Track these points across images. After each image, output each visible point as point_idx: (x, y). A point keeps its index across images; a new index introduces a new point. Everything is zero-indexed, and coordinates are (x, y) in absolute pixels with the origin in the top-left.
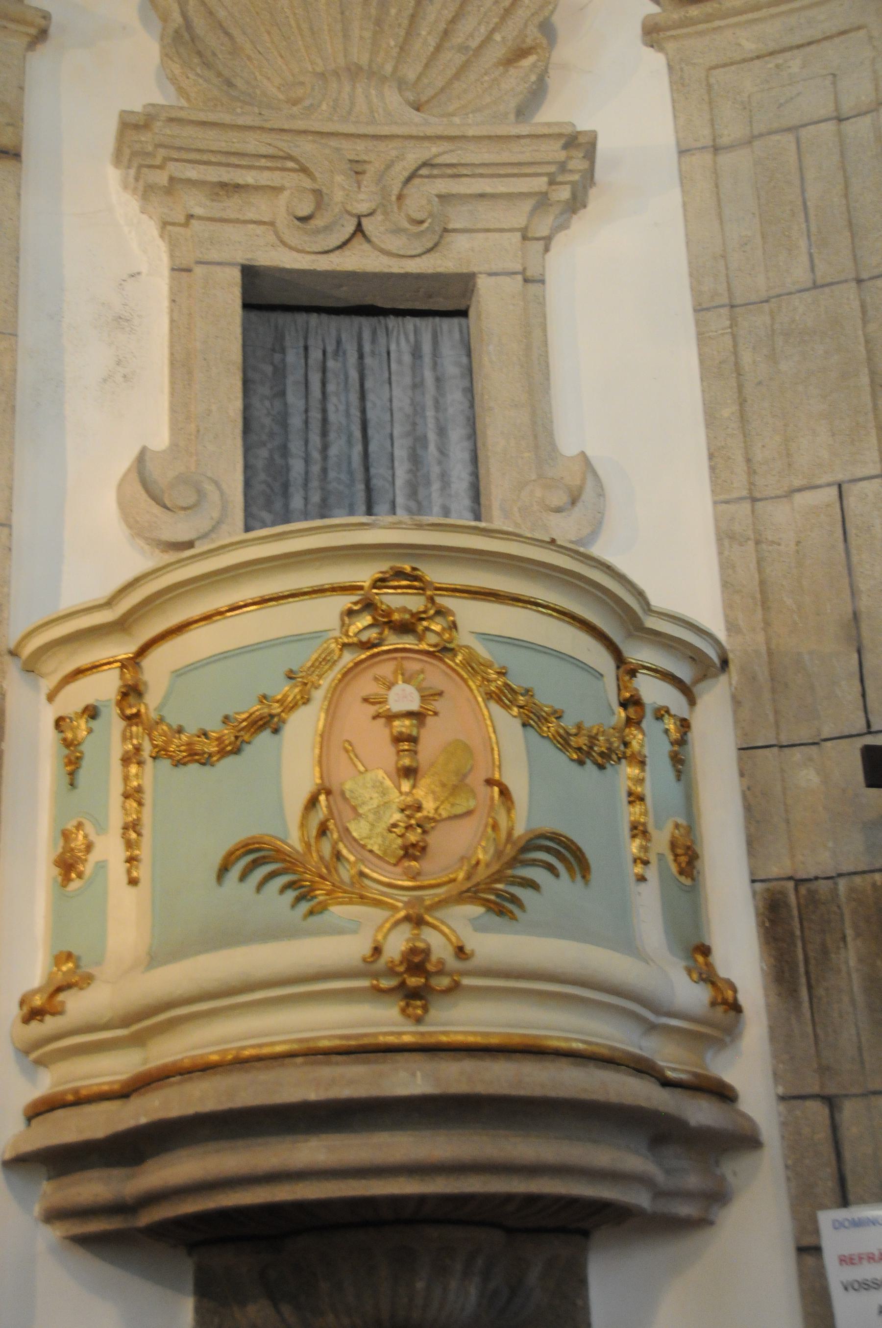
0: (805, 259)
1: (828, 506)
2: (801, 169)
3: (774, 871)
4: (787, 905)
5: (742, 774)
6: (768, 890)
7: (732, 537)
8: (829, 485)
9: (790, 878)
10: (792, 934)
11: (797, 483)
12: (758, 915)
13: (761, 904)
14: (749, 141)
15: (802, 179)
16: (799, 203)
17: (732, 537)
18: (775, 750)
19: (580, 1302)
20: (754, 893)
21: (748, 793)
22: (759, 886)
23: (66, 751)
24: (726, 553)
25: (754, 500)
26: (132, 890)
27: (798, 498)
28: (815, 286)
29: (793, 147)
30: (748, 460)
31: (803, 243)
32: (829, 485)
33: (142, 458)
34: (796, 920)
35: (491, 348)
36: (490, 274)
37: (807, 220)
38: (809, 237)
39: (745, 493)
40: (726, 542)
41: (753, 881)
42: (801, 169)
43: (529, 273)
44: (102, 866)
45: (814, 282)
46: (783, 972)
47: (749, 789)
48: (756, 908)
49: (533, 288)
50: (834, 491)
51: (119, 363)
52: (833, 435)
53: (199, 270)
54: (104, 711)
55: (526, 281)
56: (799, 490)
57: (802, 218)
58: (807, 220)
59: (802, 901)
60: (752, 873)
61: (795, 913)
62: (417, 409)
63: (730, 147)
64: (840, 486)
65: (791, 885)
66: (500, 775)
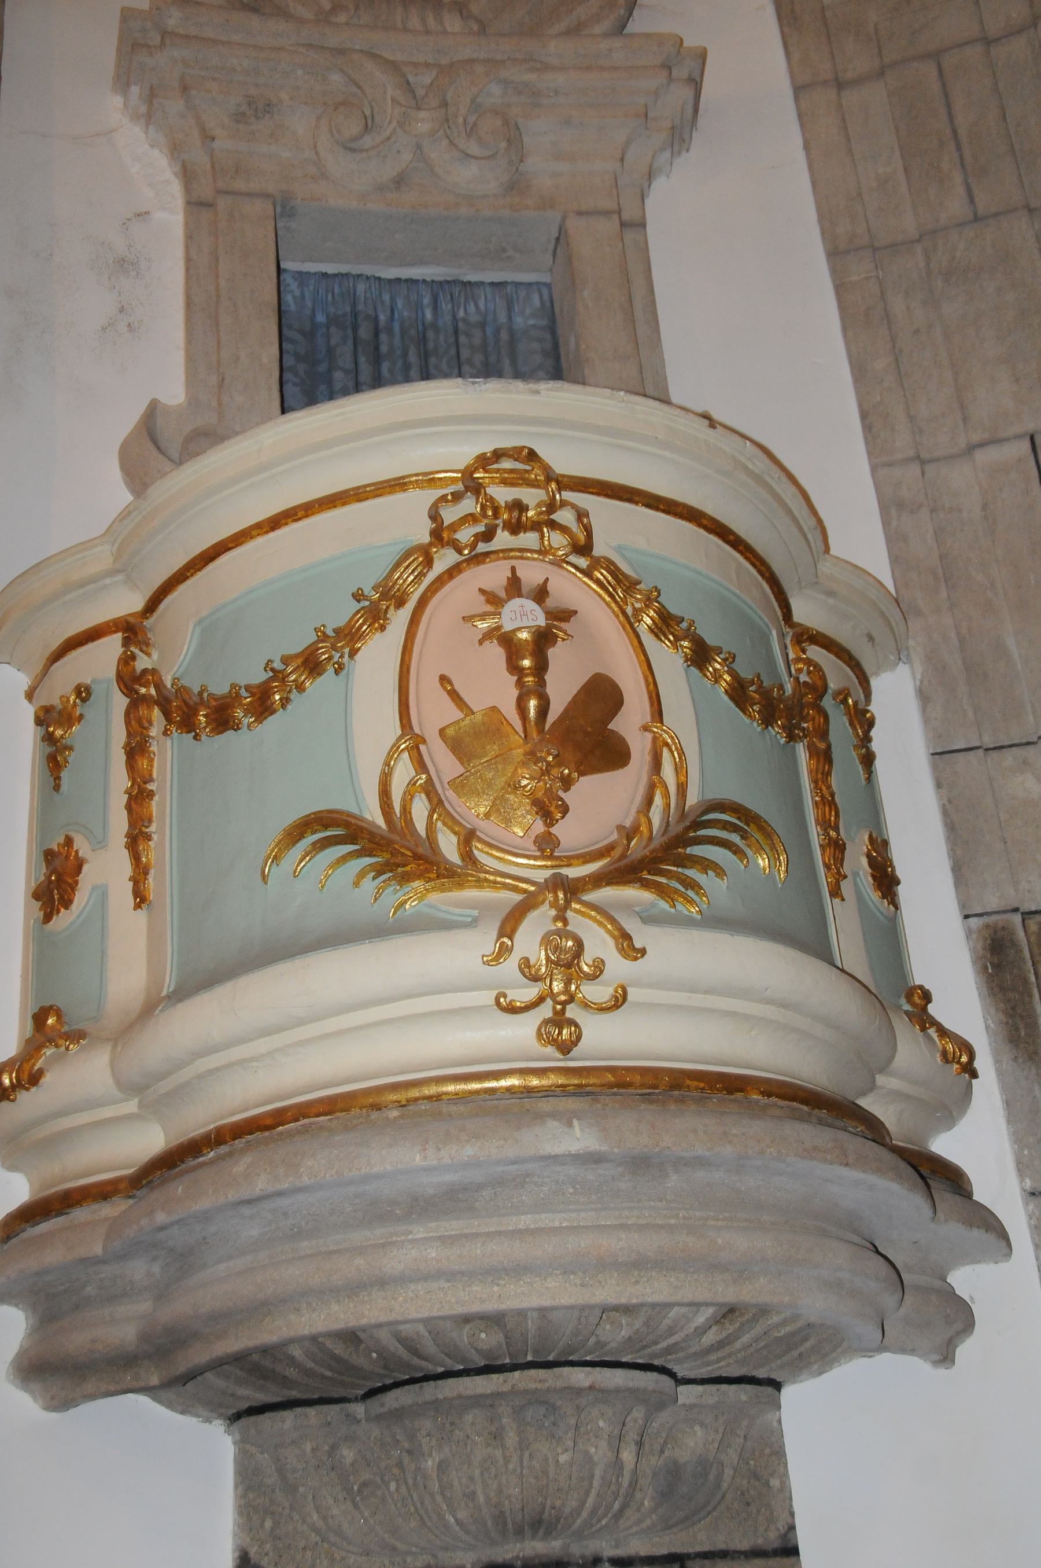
0: (960, 190)
1: (1019, 460)
2: (946, 95)
3: (993, 902)
4: (1014, 944)
5: (939, 785)
6: (987, 926)
7: (900, 505)
8: (1018, 437)
9: (1016, 910)
10: (1025, 981)
11: (976, 437)
12: (974, 962)
13: (979, 946)
14: (881, 73)
15: (949, 106)
16: (948, 131)
17: (900, 505)
18: (980, 753)
19: (775, 1483)
20: (969, 932)
21: (948, 806)
22: (974, 922)
23: (49, 750)
24: (894, 524)
25: (923, 462)
26: (142, 915)
27: (982, 457)
28: (976, 219)
29: (934, 73)
30: (911, 418)
31: (958, 178)
32: (1018, 437)
33: (153, 411)
34: (1030, 963)
35: (586, 293)
36: (580, 213)
37: (959, 148)
38: (963, 165)
39: (911, 453)
40: (894, 512)
41: (966, 917)
42: (946, 95)
43: (626, 216)
44: (102, 893)
45: (975, 214)
46: (1017, 1030)
47: (950, 801)
48: (973, 950)
49: (630, 236)
50: (1026, 445)
51: (122, 310)
52: (1017, 381)
53: (223, 203)
54: (97, 691)
55: (623, 224)
56: (982, 445)
57: (952, 147)
58: (959, 148)
59: (1033, 939)
60: (963, 905)
61: (1027, 953)
62: (411, 897)
63: (858, 81)
64: (1032, 438)
65: (1017, 919)
66: (612, 833)
